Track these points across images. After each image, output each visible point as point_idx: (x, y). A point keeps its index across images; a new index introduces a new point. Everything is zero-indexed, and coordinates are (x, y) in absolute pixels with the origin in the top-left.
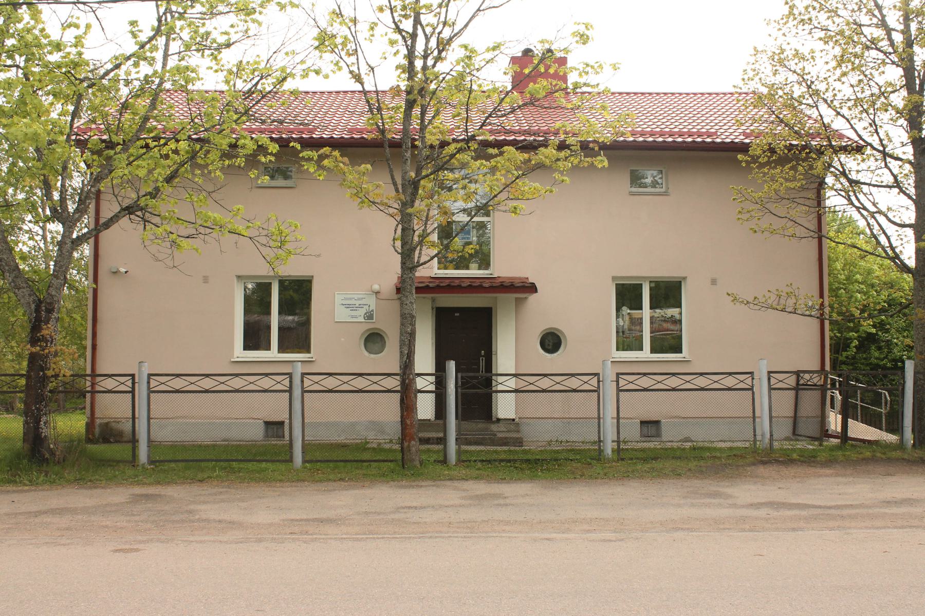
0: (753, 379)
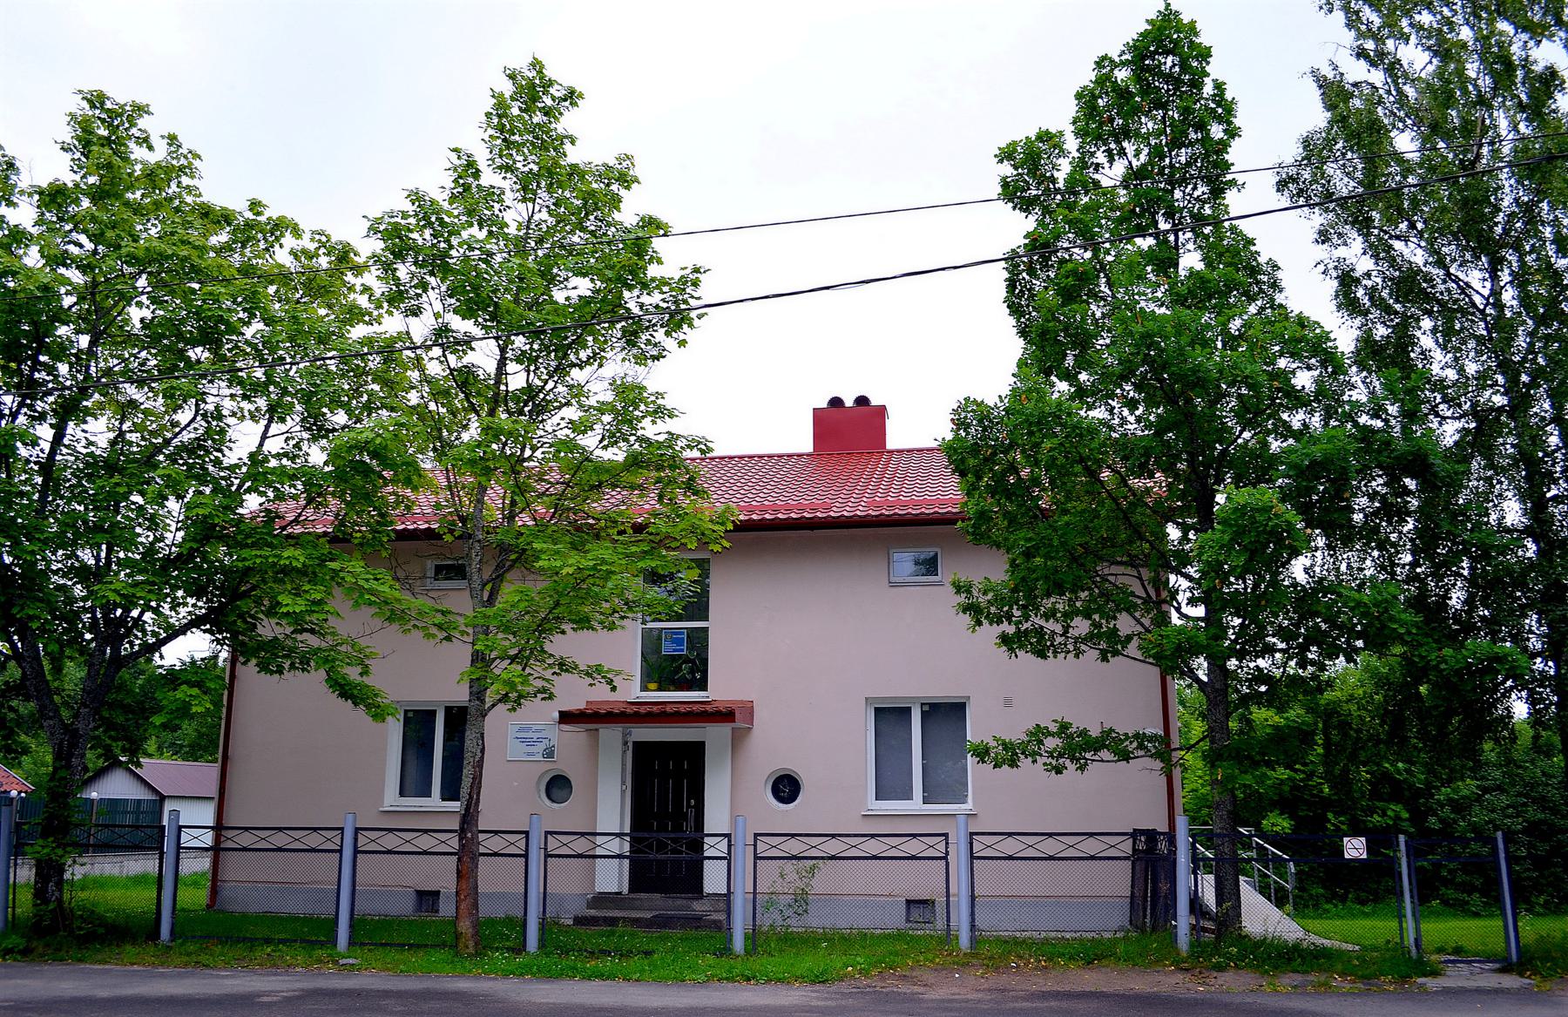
0: (947, 843)
